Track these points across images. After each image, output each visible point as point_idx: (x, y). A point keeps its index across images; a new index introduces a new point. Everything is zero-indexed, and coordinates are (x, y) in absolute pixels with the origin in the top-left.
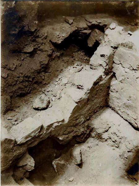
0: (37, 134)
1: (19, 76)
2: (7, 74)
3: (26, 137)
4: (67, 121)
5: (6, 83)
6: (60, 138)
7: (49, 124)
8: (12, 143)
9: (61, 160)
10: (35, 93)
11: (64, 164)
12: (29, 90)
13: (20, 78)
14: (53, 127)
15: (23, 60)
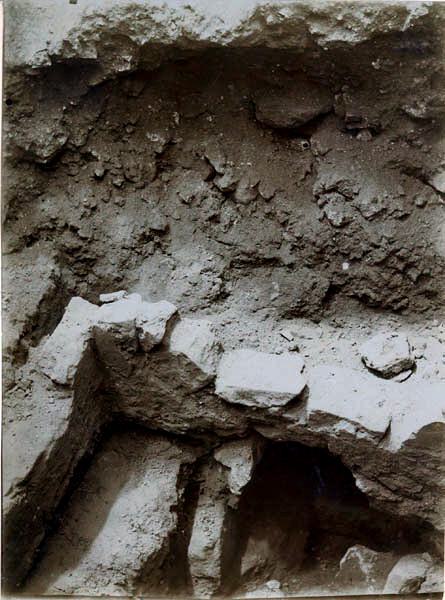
0: (274, 405)
1: (375, 242)
2: (344, 219)
3: (243, 395)
4: (396, 444)
5: (334, 242)
6: (359, 483)
7: (326, 409)
8: (199, 378)
9: (371, 560)
10: (413, 323)
11: (365, 575)
12: (399, 305)
13: (376, 250)
14: (335, 427)
15: (421, 207)
